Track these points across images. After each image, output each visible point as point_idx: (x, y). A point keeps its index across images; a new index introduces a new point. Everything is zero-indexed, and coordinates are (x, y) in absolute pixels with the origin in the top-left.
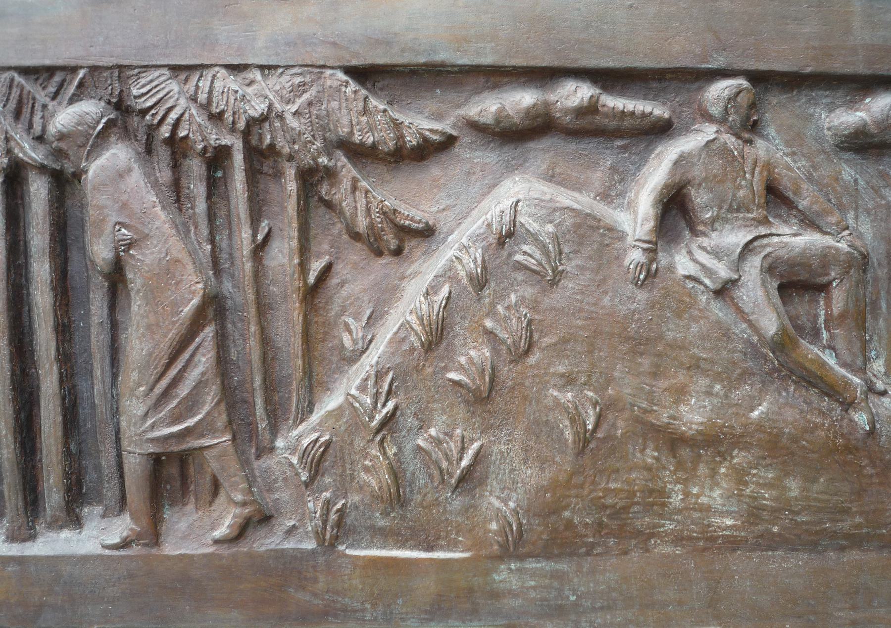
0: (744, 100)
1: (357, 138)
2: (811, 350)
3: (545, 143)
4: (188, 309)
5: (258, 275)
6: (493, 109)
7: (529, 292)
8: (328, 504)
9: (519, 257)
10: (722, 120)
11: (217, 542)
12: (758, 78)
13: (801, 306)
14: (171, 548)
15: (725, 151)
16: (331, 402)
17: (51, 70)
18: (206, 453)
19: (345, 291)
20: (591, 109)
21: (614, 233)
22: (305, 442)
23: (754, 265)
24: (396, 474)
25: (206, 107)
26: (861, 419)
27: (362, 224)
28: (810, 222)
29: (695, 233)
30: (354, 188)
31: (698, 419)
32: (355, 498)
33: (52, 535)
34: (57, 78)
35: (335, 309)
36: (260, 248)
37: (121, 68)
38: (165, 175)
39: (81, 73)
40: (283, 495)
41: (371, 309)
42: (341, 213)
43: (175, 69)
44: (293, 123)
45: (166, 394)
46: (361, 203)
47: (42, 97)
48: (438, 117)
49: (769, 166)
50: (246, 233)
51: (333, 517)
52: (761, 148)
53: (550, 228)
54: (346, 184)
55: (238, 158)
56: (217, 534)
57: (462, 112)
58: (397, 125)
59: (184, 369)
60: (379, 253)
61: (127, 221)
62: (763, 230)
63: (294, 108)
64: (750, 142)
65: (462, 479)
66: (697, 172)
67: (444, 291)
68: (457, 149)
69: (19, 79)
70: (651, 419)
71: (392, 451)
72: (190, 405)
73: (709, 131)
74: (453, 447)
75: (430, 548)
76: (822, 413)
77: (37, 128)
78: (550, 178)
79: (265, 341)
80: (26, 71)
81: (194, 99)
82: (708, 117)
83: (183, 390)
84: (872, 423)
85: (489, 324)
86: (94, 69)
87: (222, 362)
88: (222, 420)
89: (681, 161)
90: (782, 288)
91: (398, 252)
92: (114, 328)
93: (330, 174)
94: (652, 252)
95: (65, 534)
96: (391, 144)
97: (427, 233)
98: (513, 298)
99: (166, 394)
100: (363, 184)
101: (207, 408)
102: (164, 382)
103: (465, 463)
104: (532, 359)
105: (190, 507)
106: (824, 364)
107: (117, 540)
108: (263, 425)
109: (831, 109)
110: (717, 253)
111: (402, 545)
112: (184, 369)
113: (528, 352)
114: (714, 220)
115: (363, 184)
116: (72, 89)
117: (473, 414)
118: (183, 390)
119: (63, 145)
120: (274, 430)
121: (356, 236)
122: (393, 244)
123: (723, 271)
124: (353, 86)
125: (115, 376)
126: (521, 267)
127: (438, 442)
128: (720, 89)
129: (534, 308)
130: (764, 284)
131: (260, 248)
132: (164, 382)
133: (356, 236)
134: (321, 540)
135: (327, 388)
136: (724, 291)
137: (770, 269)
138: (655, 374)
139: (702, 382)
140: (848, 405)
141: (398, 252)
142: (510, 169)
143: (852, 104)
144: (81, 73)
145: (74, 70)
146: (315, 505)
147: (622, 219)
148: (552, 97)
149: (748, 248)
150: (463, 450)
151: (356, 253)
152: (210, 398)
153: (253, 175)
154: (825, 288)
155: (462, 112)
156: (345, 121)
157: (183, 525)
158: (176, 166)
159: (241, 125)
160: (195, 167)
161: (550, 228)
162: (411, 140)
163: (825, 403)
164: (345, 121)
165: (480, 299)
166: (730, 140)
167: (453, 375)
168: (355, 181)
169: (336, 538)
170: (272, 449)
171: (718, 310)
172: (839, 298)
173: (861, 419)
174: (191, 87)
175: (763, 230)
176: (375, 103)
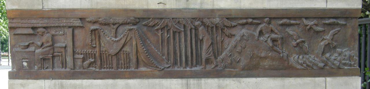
0: (268, 21)
1: (227, 25)
2: (275, 48)
3: (247, 25)
4: (210, 44)
5: (217, 39)
6: (242, 22)
7: (245, 42)
8: (224, 64)
9: (244, 38)
10: (266, 23)
11: (212, 68)
12: (270, 18)
13: (275, 43)
14: (207, 69)
15: (266, 26)
16: (224, 54)
17: (194, 18)
18: (211, 59)
19: (225, 41)
20: (252, 22)
21: (254, 35)
22: (221, 58)
23: (269, 39)
24: (231, 61)
25: (211, 22)
26: (281, 55)
27: (227, 35)
28: (276, 34)
29: (263, 35)
30: (226, 31)
31: (263, 55)
32: (227, 64)
33: (194, 68)
34: (195, 19)
35: (224, 44)
36: (217, 37)
37: (202, 18)
38: (207, 29)
39: (198, 19)
40: (219, 63)
41: (223, 38)
42: (225, 33)
43: (208, 18)
44: (220, 24)
45: (207, 53)
46: (227, 32)
47: (194, 21)
48: (235, 23)
49: (271, 28)
50: (215, 35)
51: (224, 66)
52: (271, 26)
53: (247, 35)
54: (225, 30)
55: (215, 28)
56: (212, 67)
57: (238, 22)
58: (231, 24)
59: (209, 49)
60: (229, 38)
61: (23, 58)
62: (270, 35)
63: (221, 22)
64: (269, 25)
65: (238, 62)
66: (263, 29)
67: (236, 41)
68: (237, 26)
69: (192, 19)
70: (258, 55)
71: (231, 58)
72: (210, 54)
73: (265, 24)
74: (237, 58)
75: (234, 69)
76: (277, 55)
77: (193, 24)
78: (247, 29)
79: (217, 47)
80: (192, 18)
81: (210, 21)
82: (264, 22)
83: (209, 52)
84: (283, 56)
85: (241, 45)
86: (200, 18)
87: (213, 49)
88: (213, 55)
89: (262, 28)
90: (273, 41)
91: (231, 37)
92: (201, 45)
93: (224, 29)
94: (258, 37)
95: (195, 68)
96: (231, 26)
97: (234, 35)
98: (243, 42)
99: (207, 53)
100: (228, 30)
101: (212, 54)
102: (208, 50)
103: (238, 60)
104: (246, 49)
105: (209, 64)
106: (277, 49)
107: (201, 68)
108: (217, 56)
109: (278, 21)
110: (265, 37)
111: (231, 69)
112: (209, 49)
113: (245, 48)
114: (265, 33)
115: (228, 30)
116: (197, 20)
117: (239, 54)
118: (209, 52)
119: (197, 26)
120: (218, 56)
121: (226, 36)
122: (231, 37)
123: (266, 39)
124: (226, 20)
125: (201, 51)
126: (244, 39)
127: (235, 58)
128: (266, 20)
129: (246, 43)
130: (271, 40)
131: (217, 37)
132: (208, 50)
133: (226, 36)
134: (223, 68)
135: (224, 52)
136: (266, 41)
137: (271, 39)
138: (259, 50)
139: (264, 51)
140: (280, 54)
141: (231, 37)
142: (243, 28)
143: (281, 20)
144: (198, 19)
145: (197, 18)
146: (222, 65)
147: (255, 34)
148: (247, 21)
149: (269, 37)
150: (238, 58)
151: (226, 38)
152: (212, 53)
153: (216, 29)
154: (278, 41)
155: (238, 22)
156: (226, 24)
157: (208, 67)
158: (208, 28)
159: (215, 24)
160: (210, 28)
161: (247, 35)
162: (233, 26)
163: (277, 54)
164: (226, 24)
165: (240, 42)
166: (267, 25)
167: (237, 50)
168: (226, 30)
169: (225, 68)
170: (218, 58)
171: (265, 44)
172: (279, 42)
173: (281, 55)
174: (209, 20)
175: (270, 35)
176: (229, 22)
